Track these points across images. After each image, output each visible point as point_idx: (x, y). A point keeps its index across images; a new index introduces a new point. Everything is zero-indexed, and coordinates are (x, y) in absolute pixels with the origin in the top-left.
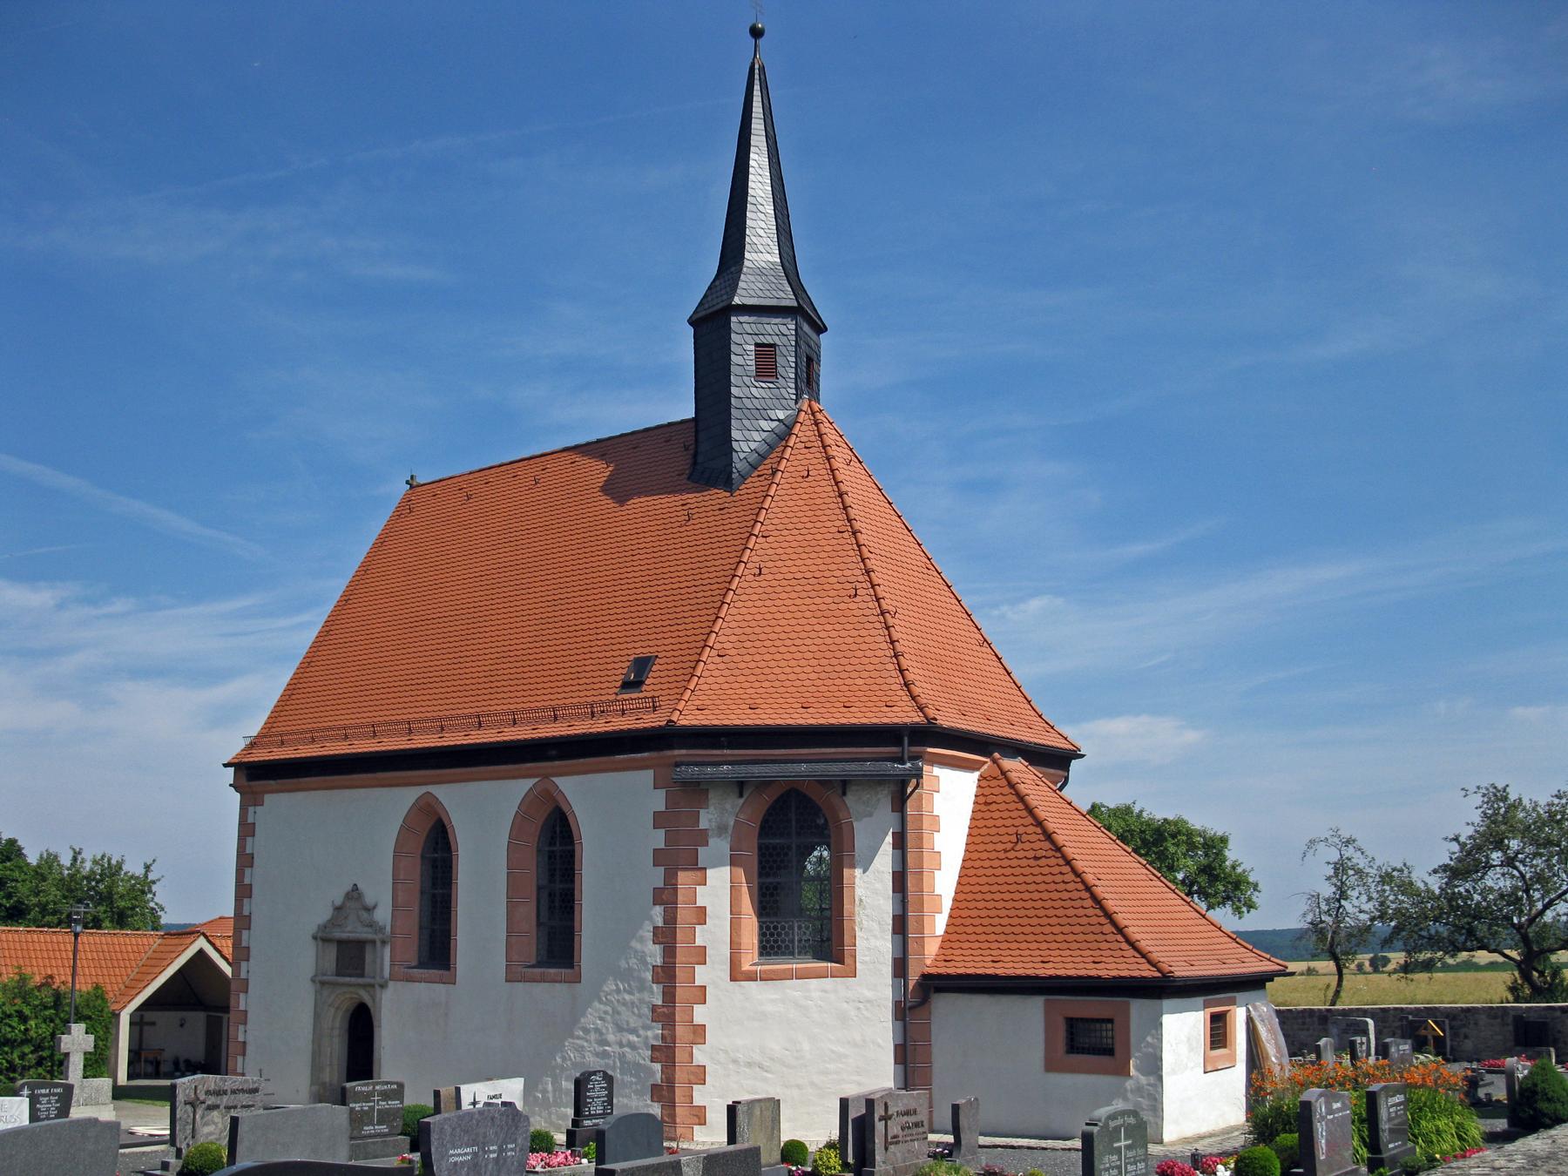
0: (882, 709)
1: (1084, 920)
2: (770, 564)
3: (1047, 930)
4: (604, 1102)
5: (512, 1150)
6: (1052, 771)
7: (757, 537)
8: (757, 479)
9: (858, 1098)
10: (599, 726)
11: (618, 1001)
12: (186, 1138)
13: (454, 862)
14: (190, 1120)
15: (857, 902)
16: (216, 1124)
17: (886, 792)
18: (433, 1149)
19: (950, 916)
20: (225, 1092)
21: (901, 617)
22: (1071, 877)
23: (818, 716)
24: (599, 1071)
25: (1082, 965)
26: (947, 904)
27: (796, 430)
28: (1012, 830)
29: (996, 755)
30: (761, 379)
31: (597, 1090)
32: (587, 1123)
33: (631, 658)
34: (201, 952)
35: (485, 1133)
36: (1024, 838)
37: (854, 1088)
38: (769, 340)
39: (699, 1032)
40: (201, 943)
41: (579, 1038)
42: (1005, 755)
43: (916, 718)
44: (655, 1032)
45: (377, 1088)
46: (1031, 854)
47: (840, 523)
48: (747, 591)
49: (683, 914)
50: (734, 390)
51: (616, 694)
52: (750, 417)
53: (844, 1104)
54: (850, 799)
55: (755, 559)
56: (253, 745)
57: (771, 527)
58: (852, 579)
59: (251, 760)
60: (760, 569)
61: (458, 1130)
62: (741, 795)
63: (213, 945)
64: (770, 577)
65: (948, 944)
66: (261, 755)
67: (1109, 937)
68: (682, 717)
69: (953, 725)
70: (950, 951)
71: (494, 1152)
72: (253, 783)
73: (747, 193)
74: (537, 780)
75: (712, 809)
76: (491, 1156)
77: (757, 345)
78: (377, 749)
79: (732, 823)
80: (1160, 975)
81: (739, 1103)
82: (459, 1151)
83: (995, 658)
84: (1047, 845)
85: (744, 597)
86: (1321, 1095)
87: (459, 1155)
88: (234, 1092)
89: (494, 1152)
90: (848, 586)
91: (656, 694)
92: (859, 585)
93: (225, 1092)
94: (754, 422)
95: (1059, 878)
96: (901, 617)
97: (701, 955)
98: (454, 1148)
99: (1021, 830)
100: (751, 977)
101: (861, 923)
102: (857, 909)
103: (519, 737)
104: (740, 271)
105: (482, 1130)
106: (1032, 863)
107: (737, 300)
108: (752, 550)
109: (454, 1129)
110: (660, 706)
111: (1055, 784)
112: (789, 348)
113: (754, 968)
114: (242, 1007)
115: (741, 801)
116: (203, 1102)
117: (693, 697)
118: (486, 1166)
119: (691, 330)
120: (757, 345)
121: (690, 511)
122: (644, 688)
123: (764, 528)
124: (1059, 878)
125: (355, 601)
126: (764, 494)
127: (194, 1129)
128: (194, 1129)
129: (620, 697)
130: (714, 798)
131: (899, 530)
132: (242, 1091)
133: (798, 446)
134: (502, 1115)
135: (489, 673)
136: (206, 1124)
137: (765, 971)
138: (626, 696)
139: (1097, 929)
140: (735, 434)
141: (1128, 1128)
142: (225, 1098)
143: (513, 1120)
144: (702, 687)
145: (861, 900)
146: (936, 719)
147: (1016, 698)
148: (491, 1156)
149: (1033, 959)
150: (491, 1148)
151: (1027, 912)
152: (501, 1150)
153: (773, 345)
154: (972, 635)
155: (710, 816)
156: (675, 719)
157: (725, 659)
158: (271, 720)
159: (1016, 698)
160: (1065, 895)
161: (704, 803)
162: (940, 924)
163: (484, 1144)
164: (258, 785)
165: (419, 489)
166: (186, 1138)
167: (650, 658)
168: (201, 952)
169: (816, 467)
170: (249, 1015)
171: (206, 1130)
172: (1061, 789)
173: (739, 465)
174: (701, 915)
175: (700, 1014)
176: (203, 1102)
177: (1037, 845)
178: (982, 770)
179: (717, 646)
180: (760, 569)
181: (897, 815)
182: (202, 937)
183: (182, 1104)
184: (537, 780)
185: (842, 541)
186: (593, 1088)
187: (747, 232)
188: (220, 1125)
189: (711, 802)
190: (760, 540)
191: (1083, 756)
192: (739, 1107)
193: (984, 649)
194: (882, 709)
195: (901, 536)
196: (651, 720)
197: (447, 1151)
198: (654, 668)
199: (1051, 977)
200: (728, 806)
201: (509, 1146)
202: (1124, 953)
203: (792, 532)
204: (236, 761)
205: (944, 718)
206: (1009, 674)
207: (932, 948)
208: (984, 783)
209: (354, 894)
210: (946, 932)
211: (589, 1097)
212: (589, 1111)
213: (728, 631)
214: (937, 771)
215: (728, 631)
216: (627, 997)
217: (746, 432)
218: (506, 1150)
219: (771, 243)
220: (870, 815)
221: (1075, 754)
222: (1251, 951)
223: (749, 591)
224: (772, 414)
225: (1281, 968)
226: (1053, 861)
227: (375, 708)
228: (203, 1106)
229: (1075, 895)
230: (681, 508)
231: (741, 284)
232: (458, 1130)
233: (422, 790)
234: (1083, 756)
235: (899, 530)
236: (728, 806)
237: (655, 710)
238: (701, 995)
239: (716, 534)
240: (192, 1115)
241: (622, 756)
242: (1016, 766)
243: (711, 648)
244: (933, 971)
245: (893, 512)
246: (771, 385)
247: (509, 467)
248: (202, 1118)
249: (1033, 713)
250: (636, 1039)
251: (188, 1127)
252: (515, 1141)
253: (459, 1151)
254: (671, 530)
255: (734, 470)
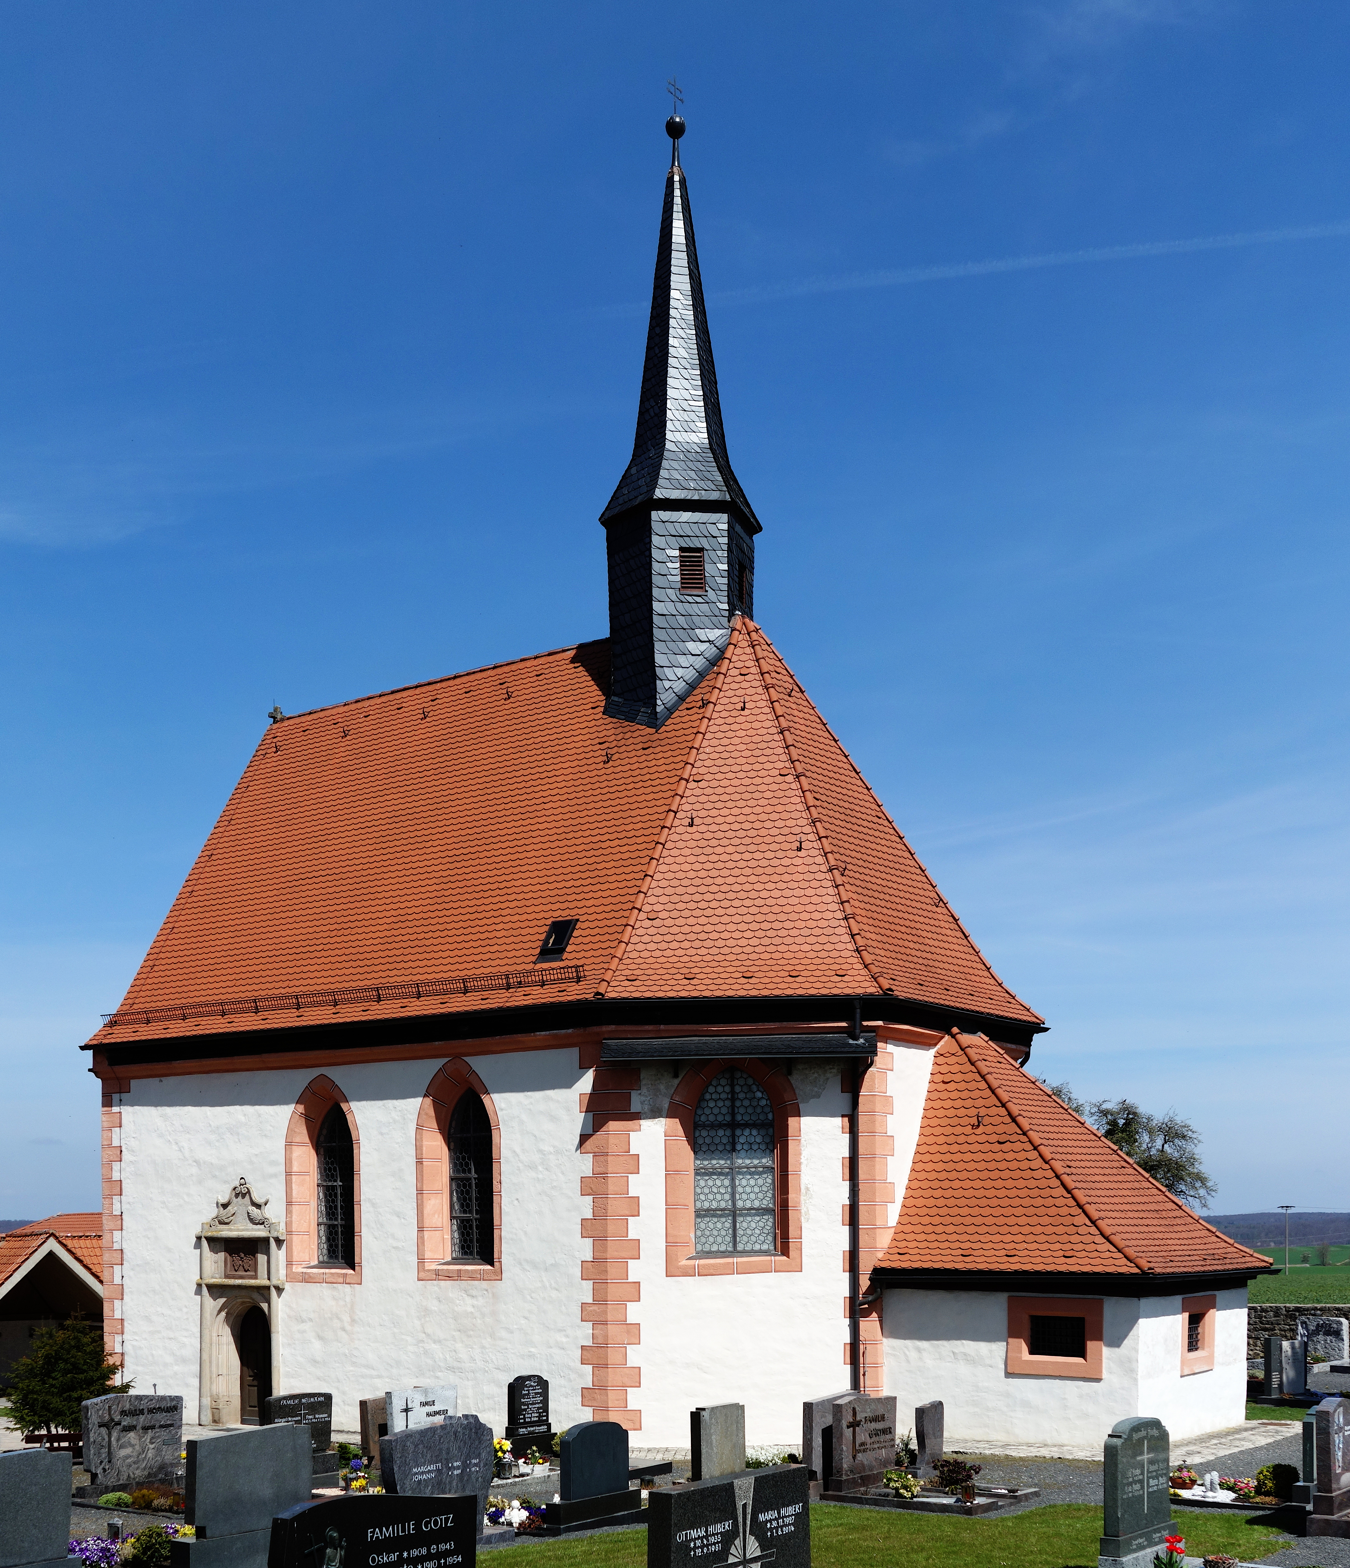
0: (832, 979)
1: (1053, 1211)
2: (703, 813)
3: (1012, 1221)
4: (539, 1408)
5: (476, 1465)
6: (1013, 1046)
7: (687, 781)
8: (685, 712)
9: (822, 1403)
10: (518, 999)
11: (544, 1299)
12: (101, 1462)
13: (355, 1151)
14: (105, 1443)
15: (803, 1190)
16: (133, 1446)
17: (835, 1071)
18: (396, 1469)
19: (904, 1206)
20: (142, 1412)
21: (851, 874)
22: (1039, 1163)
23: (761, 986)
24: (534, 1376)
25: (1051, 1260)
26: (900, 1192)
27: (728, 654)
28: (973, 1112)
29: (955, 1030)
30: (689, 592)
31: (531, 1398)
32: (522, 1431)
33: (549, 922)
34: (51, 1255)
35: (448, 1449)
36: (986, 1120)
37: (819, 1393)
38: (695, 543)
39: (634, 1332)
40: (52, 1245)
41: (501, 1339)
42: (964, 1030)
43: (871, 989)
44: (585, 1333)
45: (304, 1401)
46: (994, 1138)
47: (781, 765)
48: (678, 845)
49: (615, 1206)
50: (656, 606)
51: (535, 963)
52: (675, 638)
53: (808, 1408)
54: (795, 1079)
55: (686, 807)
56: (113, 1023)
57: (703, 770)
58: (797, 830)
59: (113, 1041)
60: (692, 819)
61: (421, 1446)
62: (676, 1076)
63: (64, 1246)
64: (703, 828)
65: (902, 1236)
66: (123, 1035)
67: (1082, 1230)
68: (610, 989)
69: (909, 996)
70: (904, 1244)
71: (458, 1468)
72: (117, 1068)
73: (668, 352)
74: (447, 1060)
75: (644, 1090)
76: (456, 1472)
77: (682, 549)
78: (262, 1027)
79: (666, 1106)
80: (1136, 1271)
81: (704, 1409)
82: (423, 1469)
83: (951, 920)
84: (1014, 1128)
85: (675, 852)
86: (1339, 1405)
87: (423, 1473)
88: (151, 1411)
89: (458, 1468)
90: (791, 838)
91: (579, 963)
92: (804, 837)
93: (142, 1412)
94: (681, 644)
95: (1025, 1165)
96: (851, 874)
97: (634, 1249)
98: (417, 1466)
99: (983, 1112)
100: (687, 1273)
101: (807, 1213)
102: (802, 1198)
103: (425, 1012)
104: (661, 457)
105: (445, 1446)
106: (997, 1147)
107: (659, 494)
108: (682, 797)
109: (416, 1446)
110: (585, 976)
111: (1016, 1060)
112: (719, 553)
113: (692, 1262)
114: (118, 1315)
115: (676, 1082)
116: (119, 1424)
117: (621, 967)
118: (450, 1483)
119: (603, 531)
120: (682, 549)
121: (609, 751)
122: (565, 955)
123: (695, 771)
124: (1025, 1165)
125: (220, 856)
126: (695, 731)
127: (110, 1453)
128: (110, 1453)
129: (538, 966)
130: (646, 1077)
131: (847, 773)
132: (160, 1409)
133: (731, 672)
134: (465, 1428)
135: (386, 939)
136: (122, 1447)
137: (704, 1266)
138: (545, 965)
139: (1068, 1220)
140: (659, 659)
141: (1151, 1439)
142: (142, 1418)
143: (476, 1433)
144: (631, 955)
145: (807, 1189)
146: (892, 990)
147: (975, 965)
148: (456, 1472)
149: (996, 1253)
150: (455, 1464)
151: (989, 1202)
152: (465, 1466)
153: (701, 550)
154: (927, 893)
155: (643, 1098)
156: (602, 991)
157: (657, 923)
158: (132, 995)
159: (975, 965)
160: (1032, 1183)
161: (635, 1084)
162: (893, 1214)
163: (448, 1461)
164: (121, 1070)
165: (286, 723)
166: (101, 1462)
167: (570, 921)
168: (51, 1255)
169: (753, 698)
170: (126, 1324)
171: (123, 1452)
172: (1022, 1064)
173: (665, 697)
174: (634, 1206)
175: (634, 1312)
176: (119, 1424)
177: (1000, 1129)
178: (938, 1046)
179: (647, 908)
180: (692, 819)
181: (847, 1096)
182: (52, 1239)
183: (96, 1427)
184: (447, 1060)
185: (784, 786)
186: (528, 1394)
187: (669, 405)
188: (137, 1448)
189: (643, 1082)
190: (692, 785)
191: (1046, 1030)
192: (702, 1413)
193: (939, 910)
194: (832, 979)
195: (848, 779)
196: (574, 993)
197: (411, 1469)
198: (575, 933)
199: (1016, 1272)
200: (662, 1087)
201: (474, 1461)
202: (1099, 1248)
203: (727, 776)
204: (95, 1042)
205: (899, 988)
206: (966, 937)
207: (884, 1240)
208: (941, 1060)
209: (242, 1192)
210: (899, 1223)
211: (524, 1404)
212: (524, 1418)
213: (658, 892)
214: (890, 1048)
215: (658, 892)
216: (554, 1294)
217: (672, 657)
218: (468, 1466)
219: (696, 419)
220: (818, 1096)
221: (1038, 1027)
222: (1232, 1245)
223: (680, 844)
224: (701, 634)
225: (1265, 1264)
226: (1018, 1146)
227: (192, 952)
228: (119, 1427)
229: (1043, 1183)
230: (599, 746)
231: (663, 473)
232: (421, 1446)
233: (315, 1072)
234: (1046, 1030)
235: (847, 773)
236: (662, 1087)
237: (577, 982)
238: (635, 1292)
239: (640, 778)
240: (106, 1437)
241: (563, 1031)
242: (977, 1040)
243: (640, 910)
244: (884, 1265)
245: (839, 751)
246: (699, 599)
247: (391, 697)
248: (118, 1440)
249: (992, 982)
250: (564, 1340)
251: (103, 1450)
252: (478, 1456)
253: (423, 1469)
254: (587, 774)
255: (659, 702)
